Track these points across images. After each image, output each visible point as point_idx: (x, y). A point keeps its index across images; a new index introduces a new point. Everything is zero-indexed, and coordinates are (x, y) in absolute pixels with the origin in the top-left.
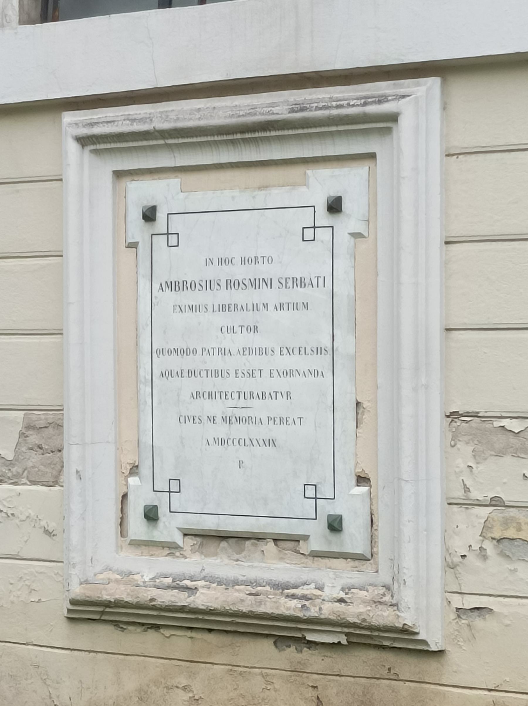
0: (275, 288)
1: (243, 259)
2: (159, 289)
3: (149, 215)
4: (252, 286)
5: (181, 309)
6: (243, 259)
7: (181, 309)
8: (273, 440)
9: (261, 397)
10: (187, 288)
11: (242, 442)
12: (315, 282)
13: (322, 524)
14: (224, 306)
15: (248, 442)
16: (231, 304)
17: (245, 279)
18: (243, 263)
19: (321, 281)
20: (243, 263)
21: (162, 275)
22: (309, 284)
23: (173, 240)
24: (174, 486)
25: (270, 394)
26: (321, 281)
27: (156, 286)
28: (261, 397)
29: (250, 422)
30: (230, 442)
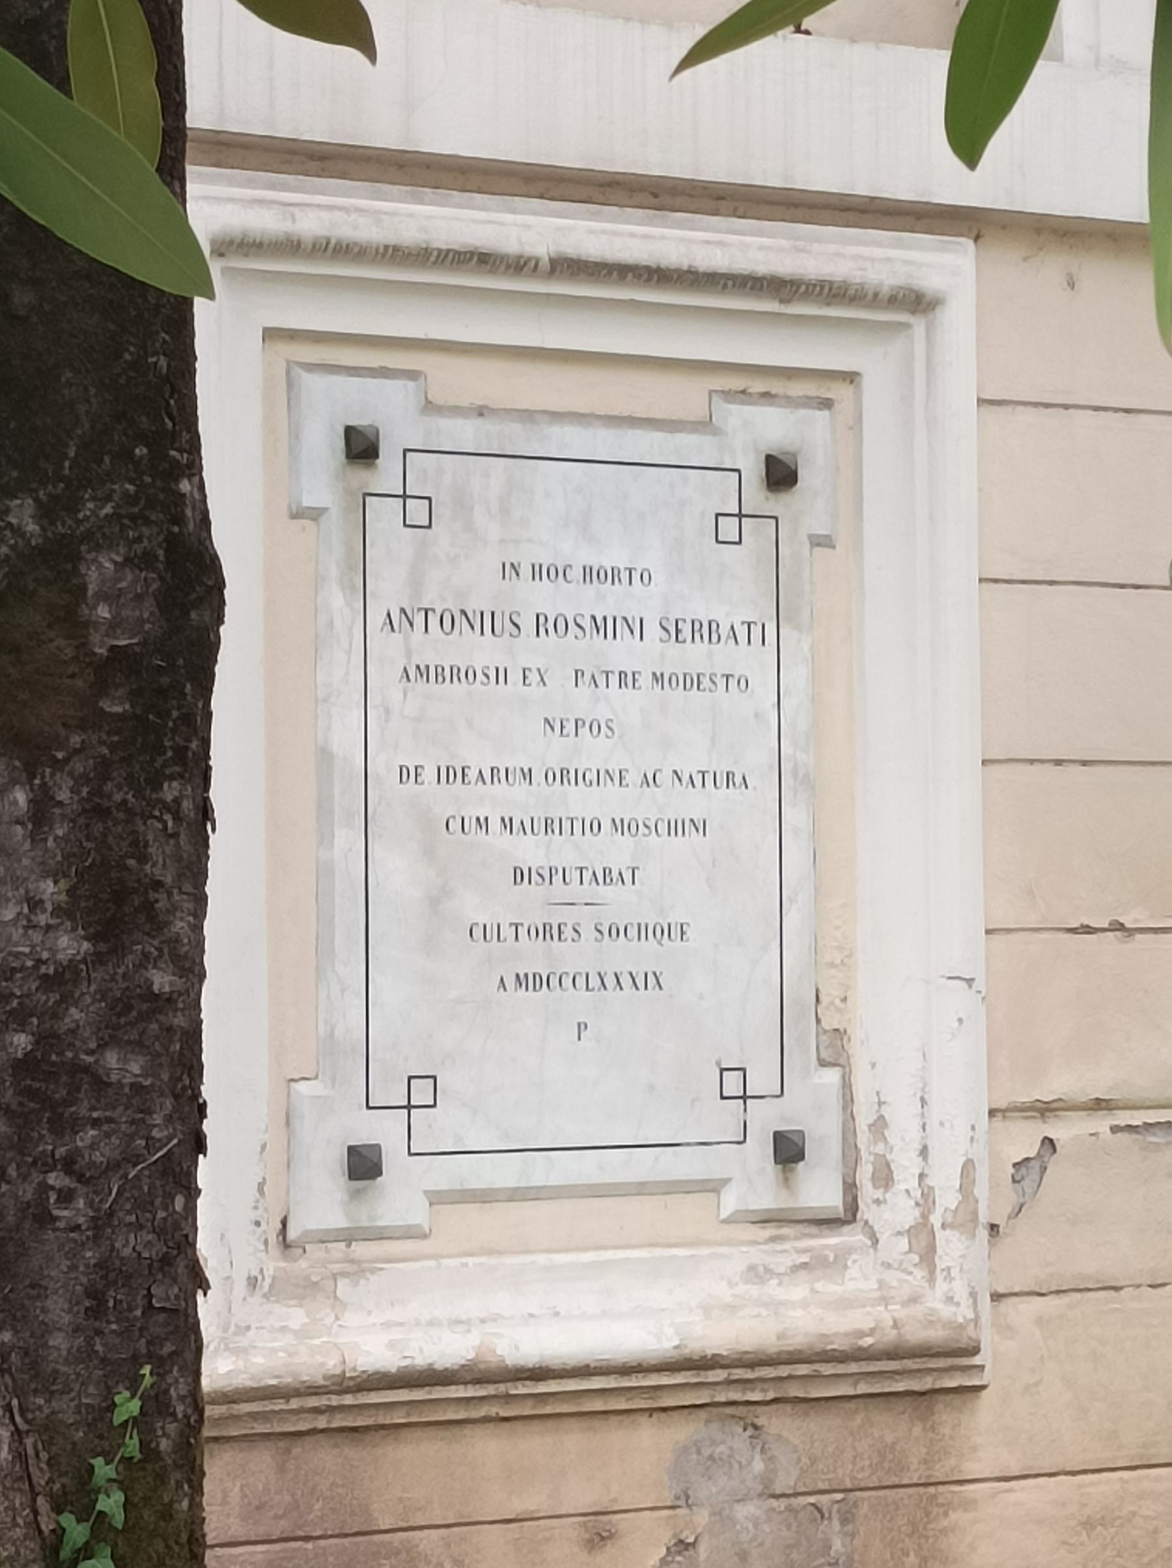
0: (653, 640)
1: (537, 568)
2: (385, 624)
3: (361, 448)
4: (598, 631)
5: (542, 679)
6: (537, 568)
7: (542, 679)
8: (655, 974)
9: (601, 880)
10: (547, 631)
11: (580, 982)
12: (742, 632)
13: (760, 1150)
14: (440, 670)
15: (594, 982)
16: (704, 675)
17: (583, 616)
18: (588, 578)
19: (756, 631)
20: (588, 578)
21: (389, 590)
22: (728, 637)
23: (417, 511)
24: (420, 1094)
25: (620, 874)
26: (756, 631)
27: (376, 618)
28: (601, 880)
29: (548, 936)
30: (554, 981)
